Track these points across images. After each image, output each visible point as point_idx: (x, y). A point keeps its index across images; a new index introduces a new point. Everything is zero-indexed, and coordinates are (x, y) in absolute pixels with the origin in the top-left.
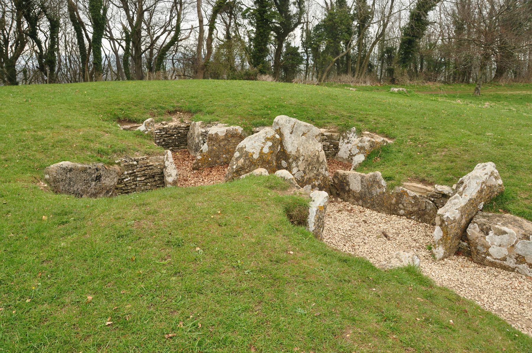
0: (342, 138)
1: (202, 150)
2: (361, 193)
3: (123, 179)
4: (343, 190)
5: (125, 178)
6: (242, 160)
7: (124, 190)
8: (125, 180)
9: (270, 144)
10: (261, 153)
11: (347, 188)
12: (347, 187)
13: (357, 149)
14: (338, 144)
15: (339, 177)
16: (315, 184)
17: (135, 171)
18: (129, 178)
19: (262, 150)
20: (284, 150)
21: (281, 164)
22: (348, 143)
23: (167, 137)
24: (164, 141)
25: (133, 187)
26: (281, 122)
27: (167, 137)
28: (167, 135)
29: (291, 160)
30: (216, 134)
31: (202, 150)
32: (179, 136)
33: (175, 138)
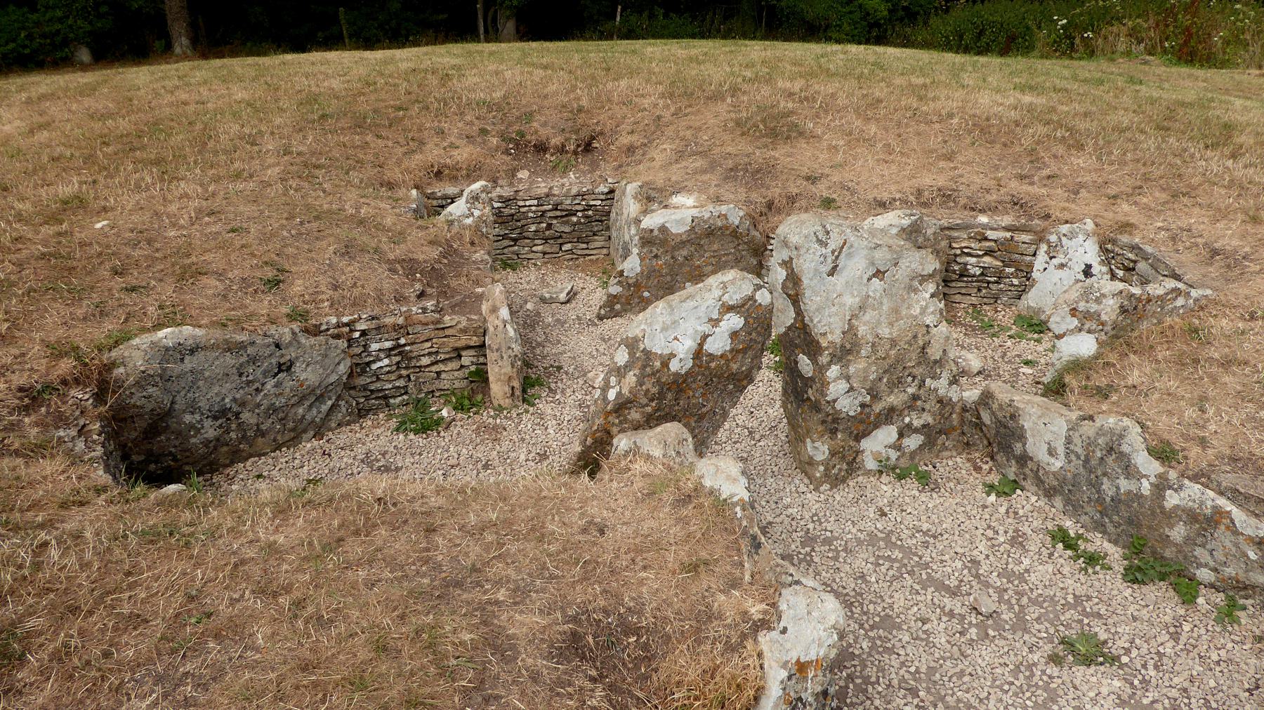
0: (1044, 247)
1: (622, 271)
2: (1060, 477)
3: (368, 364)
4: (1007, 448)
5: (374, 362)
6: (631, 378)
7: (372, 391)
8: (374, 367)
9: (734, 321)
10: (698, 353)
11: (1018, 448)
12: (1019, 445)
13: (1069, 318)
14: (1031, 265)
15: (995, 406)
16: (909, 426)
17: (402, 341)
18: (386, 361)
19: (701, 345)
20: (805, 326)
21: (796, 363)
22: (1062, 266)
23: (556, 217)
24: (549, 226)
25: (401, 383)
26: (794, 239)
27: (556, 217)
28: (558, 213)
29: (824, 359)
30: (663, 229)
31: (622, 271)
32: (587, 217)
33: (579, 223)
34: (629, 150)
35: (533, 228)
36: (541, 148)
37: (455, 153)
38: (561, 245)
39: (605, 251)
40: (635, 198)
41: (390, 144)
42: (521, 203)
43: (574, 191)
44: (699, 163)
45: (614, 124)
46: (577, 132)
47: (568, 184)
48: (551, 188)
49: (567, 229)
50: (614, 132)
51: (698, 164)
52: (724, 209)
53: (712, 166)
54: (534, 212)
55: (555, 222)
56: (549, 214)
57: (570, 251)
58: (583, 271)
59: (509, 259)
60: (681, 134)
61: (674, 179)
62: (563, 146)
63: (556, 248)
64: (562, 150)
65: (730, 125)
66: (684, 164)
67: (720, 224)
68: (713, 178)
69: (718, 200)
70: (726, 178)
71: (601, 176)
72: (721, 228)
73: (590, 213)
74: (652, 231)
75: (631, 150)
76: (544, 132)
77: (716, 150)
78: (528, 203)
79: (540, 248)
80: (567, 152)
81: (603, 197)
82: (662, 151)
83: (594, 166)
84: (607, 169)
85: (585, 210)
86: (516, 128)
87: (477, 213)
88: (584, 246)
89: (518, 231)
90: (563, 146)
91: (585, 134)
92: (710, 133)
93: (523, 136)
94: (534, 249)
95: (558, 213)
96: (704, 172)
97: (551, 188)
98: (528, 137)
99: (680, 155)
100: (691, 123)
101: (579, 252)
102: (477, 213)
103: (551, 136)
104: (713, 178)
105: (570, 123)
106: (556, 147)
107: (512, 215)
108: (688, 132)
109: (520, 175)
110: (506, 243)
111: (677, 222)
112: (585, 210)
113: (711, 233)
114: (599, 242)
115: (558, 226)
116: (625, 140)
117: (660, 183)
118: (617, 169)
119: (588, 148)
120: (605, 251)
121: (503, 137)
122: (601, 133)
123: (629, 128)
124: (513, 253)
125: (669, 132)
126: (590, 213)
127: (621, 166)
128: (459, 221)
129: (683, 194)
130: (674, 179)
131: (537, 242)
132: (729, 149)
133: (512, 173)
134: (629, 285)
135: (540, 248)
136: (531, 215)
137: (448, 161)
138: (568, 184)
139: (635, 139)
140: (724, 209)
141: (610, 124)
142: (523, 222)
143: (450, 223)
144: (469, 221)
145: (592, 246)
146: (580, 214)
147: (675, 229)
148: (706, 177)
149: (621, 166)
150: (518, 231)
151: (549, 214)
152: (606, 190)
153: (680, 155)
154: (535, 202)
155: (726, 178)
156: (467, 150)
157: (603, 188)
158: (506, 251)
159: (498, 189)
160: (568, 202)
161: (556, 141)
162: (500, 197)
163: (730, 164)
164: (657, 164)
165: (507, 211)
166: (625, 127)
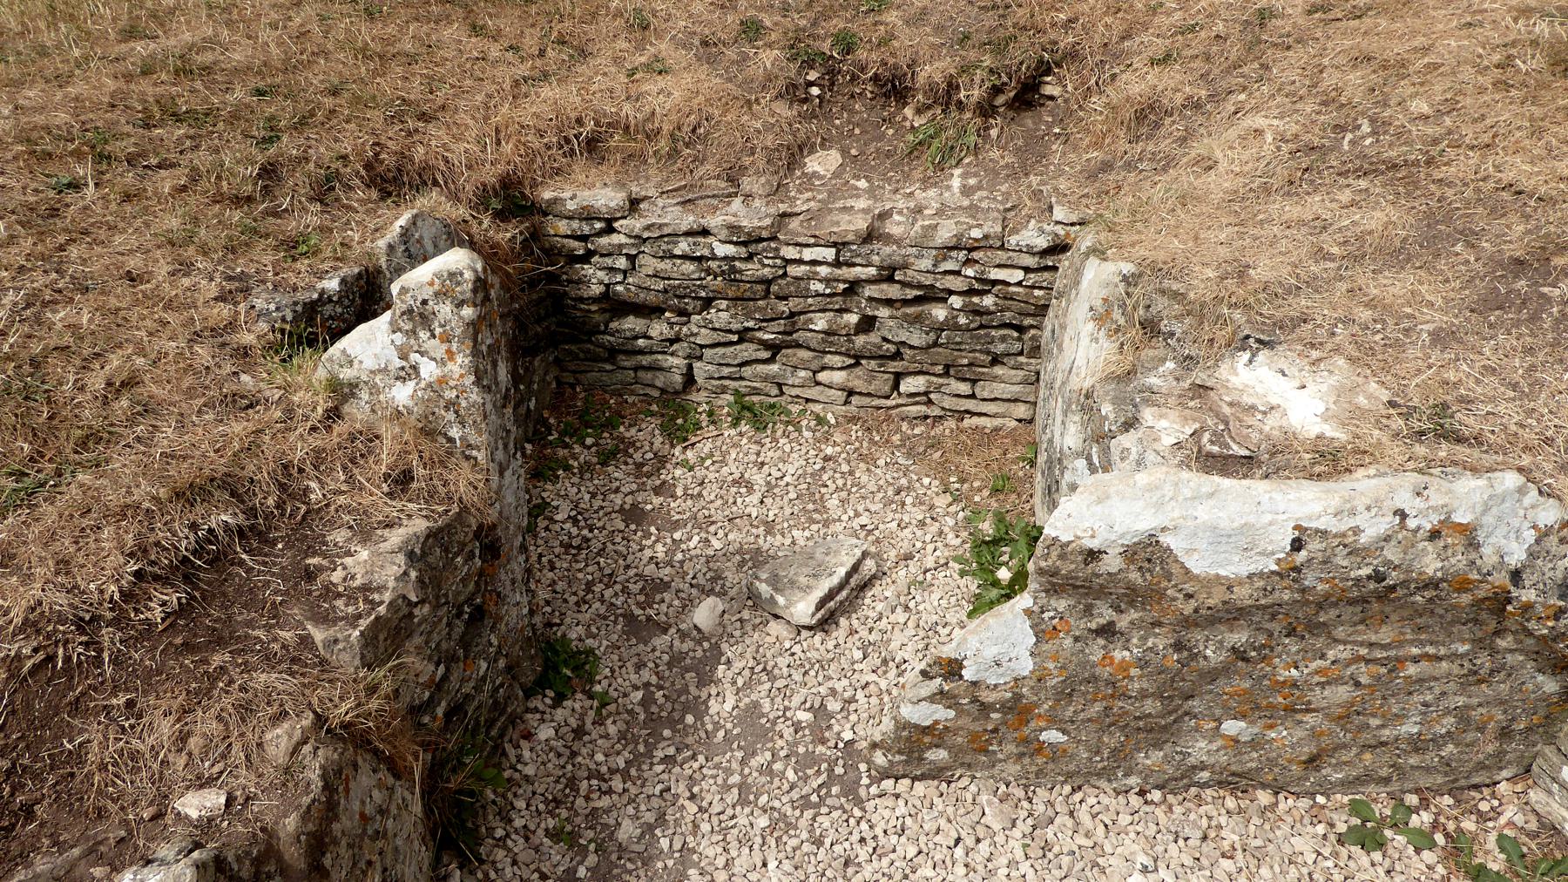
23: (889, 302)
24: (867, 324)
27: (889, 302)
28: (893, 291)
30: (1148, 552)
32: (978, 312)
33: (950, 325)
34: (1140, 117)
35: (821, 322)
36: (894, 88)
37: (651, 86)
38: (898, 377)
39: (1021, 411)
40: (1101, 318)
41: (494, 51)
42: (790, 252)
43: (945, 234)
44: (1382, 216)
45: (1118, 28)
46: (999, 47)
47: (934, 210)
48: (884, 216)
49: (917, 338)
50: (1113, 54)
51: (1374, 219)
52: (1465, 496)
53: (1435, 236)
54: (827, 281)
55: (883, 312)
56: (869, 291)
57: (925, 397)
58: (942, 470)
59: (756, 392)
60: (1330, 80)
61: (1262, 271)
62: (952, 87)
63: (882, 383)
64: (946, 98)
65: (1530, 64)
66: (1316, 204)
67: (1431, 565)
68: (1426, 295)
69: (1439, 431)
70: (1491, 303)
71: (1036, 195)
72: (1433, 584)
73: (988, 301)
74: (1093, 555)
75: (1147, 116)
76: (908, 41)
77: (1461, 166)
78: (808, 254)
79: (838, 377)
80: (960, 106)
81: (1031, 261)
82: (1245, 141)
83: (1032, 155)
84: (1066, 165)
85: (971, 292)
86: (837, 24)
87: (428, 370)
88: (964, 388)
89: (780, 325)
90: (952, 87)
91: (1022, 55)
92: (1439, 88)
93: (848, 50)
94: (822, 376)
95: (893, 291)
96: (1396, 256)
97: (884, 216)
98: (862, 54)
99: (1309, 163)
100: (1372, 45)
101: (948, 403)
102: (428, 370)
103: (924, 52)
104: (1426, 295)
105: (990, 20)
106: (931, 88)
107: (767, 282)
108: (1355, 77)
109: (813, 164)
110: (748, 351)
111: (1219, 537)
112: (971, 292)
113: (1380, 596)
114: (1005, 382)
115: (890, 325)
116: (1136, 84)
117: (1202, 281)
118: (1092, 176)
119: (1027, 96)
120: (1021, 411)
121: (800, 52)
122: (1073, 55)
123: (1160, 46)
124: (765, 379)
125: (1289, 68)
126: (988, 301)
127: (1106, 167)
128: (375, 390)
129: (1284, 356)
130: (1262, 271)
131: (831, 360)
132: (1517, 169)
133: (794, 154)
134: (985, 708)
135: (838, 377)
136: (817, 286)
137: (627, 108)
138: (934, 210)
139: (1172, 83)
140: (1465, 496)
141: (1107, 27)
142: (794, 304)
143: (342, 392)
144: (402, 394)
145: (983, 390)
146: (956, 301)
147: (1200, 560)
148: (1395, 286)
149: (1106, 167)
150: (780, 325)
151: (869, 291)
152: (1042, 243)
153: (1309, 163)
154: (830, 254)
155: (1491, 303)
156: (687, 79)
157: (1034, 236)
158: (747, 371)
159: (737, 204)
160: (926, 264)
161: (932, 72)
162: (733, 228)
163: (1516, 236)
164: (1218, 184)
165: (752, 270)
166: (1151, 42)
